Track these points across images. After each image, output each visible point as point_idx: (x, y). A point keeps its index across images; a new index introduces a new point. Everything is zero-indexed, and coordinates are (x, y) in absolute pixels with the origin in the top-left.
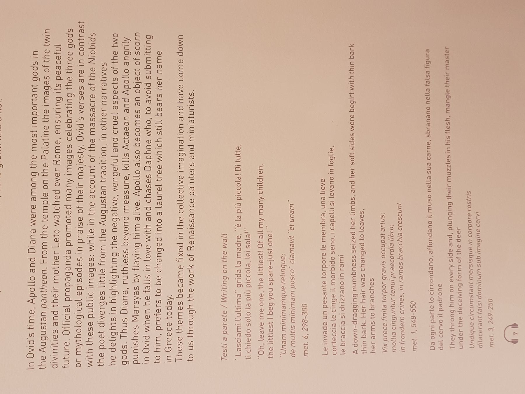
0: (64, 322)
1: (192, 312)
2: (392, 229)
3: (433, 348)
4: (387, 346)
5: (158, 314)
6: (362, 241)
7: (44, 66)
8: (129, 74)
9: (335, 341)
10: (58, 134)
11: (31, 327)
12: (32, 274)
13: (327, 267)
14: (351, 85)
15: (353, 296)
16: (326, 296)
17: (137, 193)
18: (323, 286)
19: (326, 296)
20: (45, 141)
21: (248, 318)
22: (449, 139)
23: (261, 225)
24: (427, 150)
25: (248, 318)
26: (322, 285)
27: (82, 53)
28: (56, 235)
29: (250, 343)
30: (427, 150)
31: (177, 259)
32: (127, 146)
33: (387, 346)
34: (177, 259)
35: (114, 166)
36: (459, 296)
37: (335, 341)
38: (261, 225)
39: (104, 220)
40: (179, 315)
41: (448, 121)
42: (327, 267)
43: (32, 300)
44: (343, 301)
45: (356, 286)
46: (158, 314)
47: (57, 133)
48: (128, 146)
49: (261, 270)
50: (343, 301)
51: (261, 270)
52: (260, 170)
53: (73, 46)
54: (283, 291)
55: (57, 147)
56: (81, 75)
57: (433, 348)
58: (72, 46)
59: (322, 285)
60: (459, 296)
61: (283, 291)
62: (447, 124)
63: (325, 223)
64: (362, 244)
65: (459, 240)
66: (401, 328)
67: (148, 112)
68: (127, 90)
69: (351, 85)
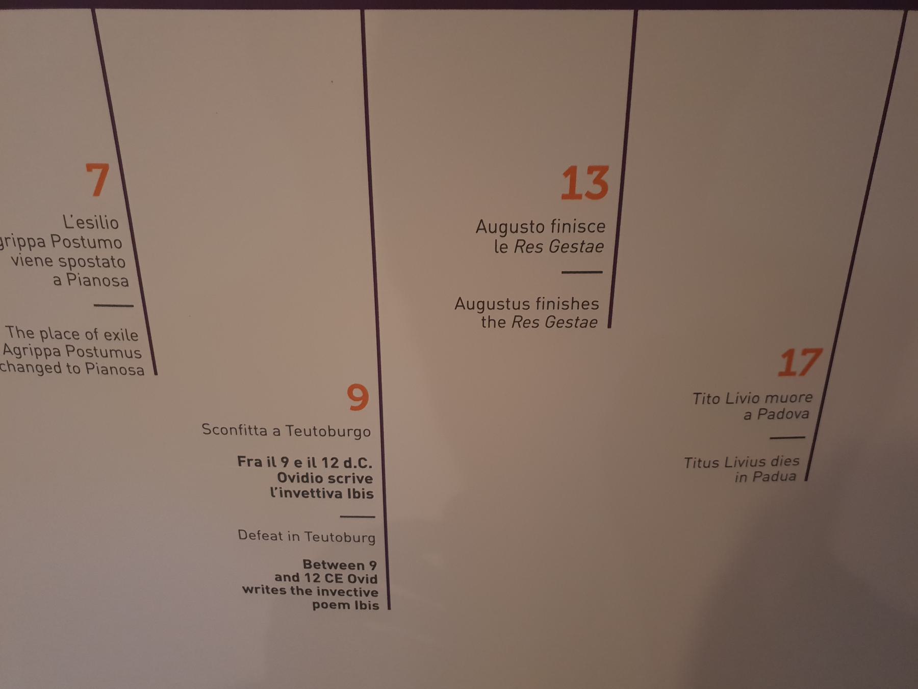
0: (559, 222)
1: (358, 434)
3: (243, 536)
5: (261, 536)
7: (97, 331)
11: (556, 227)
14: (18, 258)
15: (479, 302)
17: (461, 305)
20: (111, 262)
28: (115, 262)
29: (312, 482)
31: (557, 220)
32: (485, 229)
34: (557, 220)
35: (257, 535)
36: (358, 477)
39: (466, 307)
43: (461, 305)
46: (261, 536)
49: (332, 539)
51: (332, 539)
53: (482, 310)
54: (800, 399)
55: (489, 307)
56: (804, 398)
57: (243, 536)
58: (481, 309)
60: (358, 477)
61: (800, 399)
63: (483, 302)
66: (783, 412)
68: (45, 356)
69: (18, 258)
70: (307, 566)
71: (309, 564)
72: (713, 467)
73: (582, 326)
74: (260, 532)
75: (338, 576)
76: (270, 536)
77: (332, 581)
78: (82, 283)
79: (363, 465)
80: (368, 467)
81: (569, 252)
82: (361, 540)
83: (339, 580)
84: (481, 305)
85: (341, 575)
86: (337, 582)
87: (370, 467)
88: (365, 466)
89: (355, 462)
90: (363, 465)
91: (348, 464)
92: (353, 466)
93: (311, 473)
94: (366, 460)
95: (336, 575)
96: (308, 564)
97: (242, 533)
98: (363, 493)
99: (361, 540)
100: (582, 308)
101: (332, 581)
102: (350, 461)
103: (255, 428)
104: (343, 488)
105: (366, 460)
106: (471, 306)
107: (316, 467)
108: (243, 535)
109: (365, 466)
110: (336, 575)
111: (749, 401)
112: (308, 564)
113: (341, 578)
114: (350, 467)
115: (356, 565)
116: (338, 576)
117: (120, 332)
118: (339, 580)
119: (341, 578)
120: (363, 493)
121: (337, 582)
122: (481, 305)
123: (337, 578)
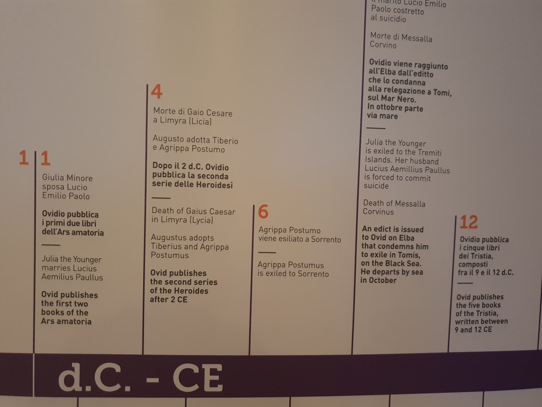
2: (293, 273)
4: (273, 272)
6: (288, 273)
8: (177, 240)
9: (171, 112)
10: (266, 274)
12: (185, 140)
13: (197, 244)
16: (413, 206)
18: (298, 238)
19: (413, 206)
21: (75, 295)
22: (415, 256)
23: (51, 197)
24: (310, 273)
25: (75, 295)
26: (444, 65)
27: (408, 179)
30: (310, 273)
33: (273, 272)
37: (171, 112)
38: (51, 197)
39: (158, 139)
40: (433, 3)
41: (194, 274)
42: (197, 244)
44: (496, 273)
45: (51, 179)
47: (267, 273)
48: (204, 249)
50: (496, 273)
52: (318, 274)
53: (92, 263)
59: (444, 65)
62: (204, 272)
64: (284, 274)
65: (374, 272)
67: (291, 274)
70: (388, 264)
71: (389, 263)
72: (204, 214)
73: (193, 213)
74: (183, 209)
75: (185, 298)
76: (373, 203)
77: (181, 301)
78: (205, 123)
79: (198, 167)
80: (201, 169)
81: (228, 211)
82: (309, 232)
83: (185, 301)
84: (163, 238)
85: (187, 297)
86: (184, 302)
87: (202, 169)
88: (200, 168)
89: (194, 166)
90: (198, 167)
91: (191, 167)
92: (193, 168)
93: (176, 172)
94: (200, 165)
95: (184, 297)
96: (388, 263)
97: (154, 209)
98: (414, 254)
99: (309, 232)
100: (423, 37)
101: (181, 301)
102: (192, 165)
103: (204, 139)
104: (194, 181)
105: (200, 165)
106: (159, 238)
107: (179, 168)
108: (155, 210)
109: (200, 168)
110: (184, 297)
111: (407, 39)
112: (388, 263)
113: (186, 299)
114: (192, 168)
115: (161, 183)
116: (185, 298)
117: (379, 253)
118: (185, 301)
119: (186, 299)
120: (414, 254)
121: (184, 302)
122: (163, 238)
123: (184, 299)
